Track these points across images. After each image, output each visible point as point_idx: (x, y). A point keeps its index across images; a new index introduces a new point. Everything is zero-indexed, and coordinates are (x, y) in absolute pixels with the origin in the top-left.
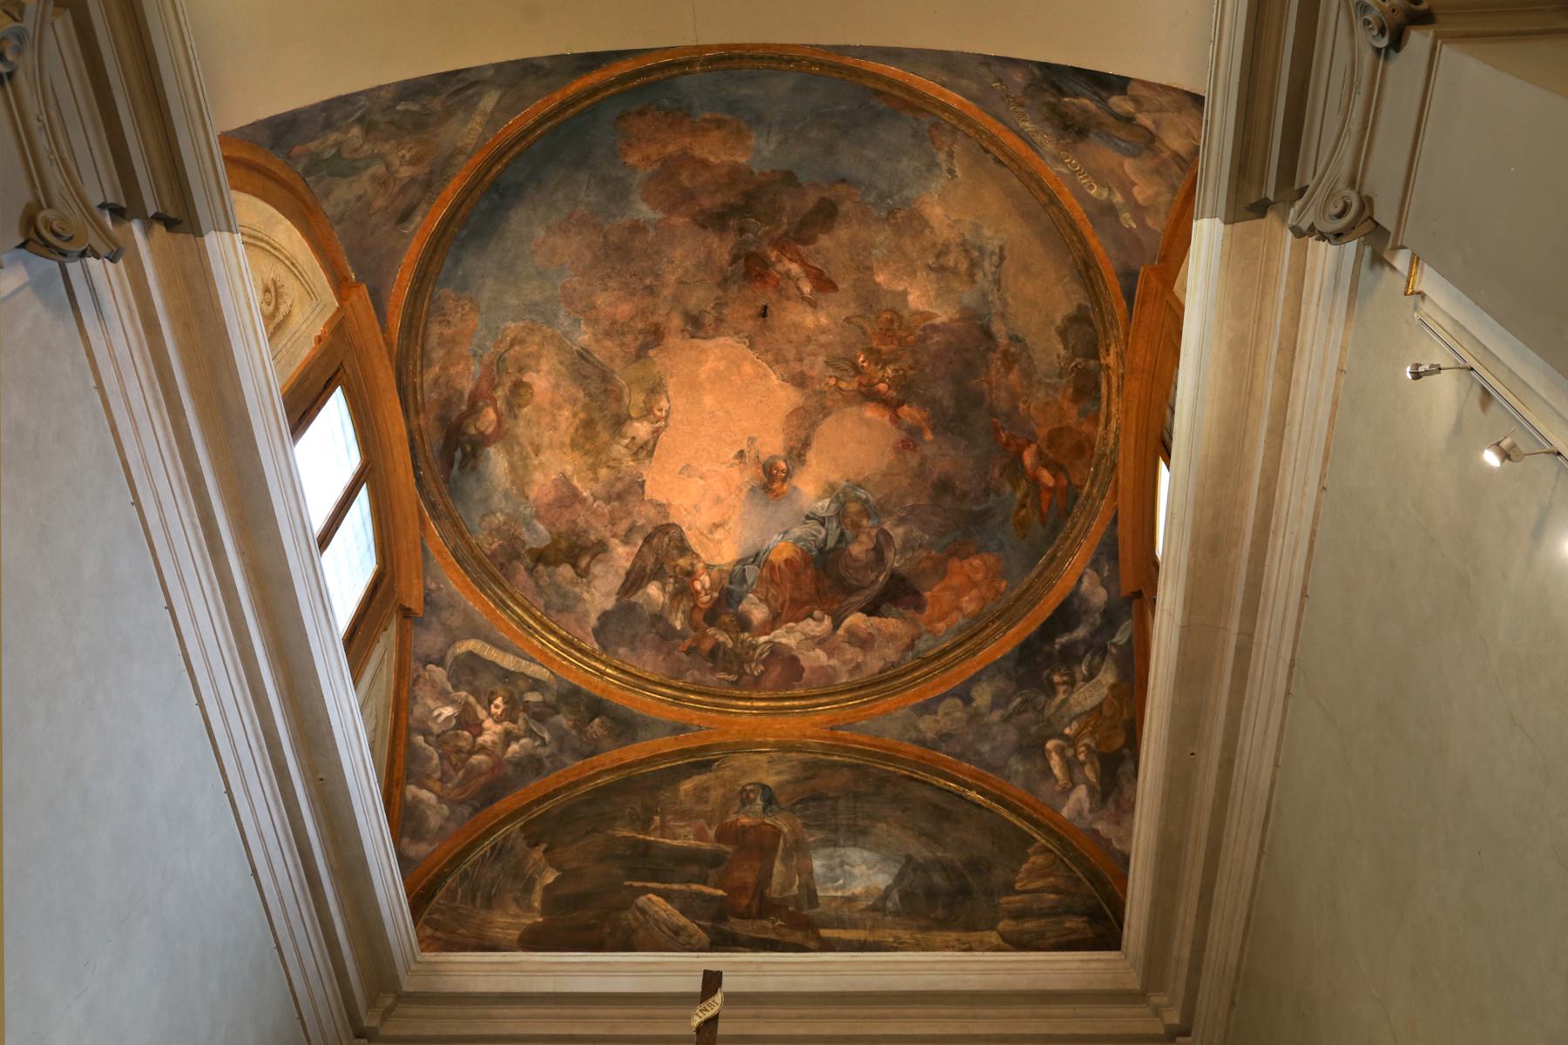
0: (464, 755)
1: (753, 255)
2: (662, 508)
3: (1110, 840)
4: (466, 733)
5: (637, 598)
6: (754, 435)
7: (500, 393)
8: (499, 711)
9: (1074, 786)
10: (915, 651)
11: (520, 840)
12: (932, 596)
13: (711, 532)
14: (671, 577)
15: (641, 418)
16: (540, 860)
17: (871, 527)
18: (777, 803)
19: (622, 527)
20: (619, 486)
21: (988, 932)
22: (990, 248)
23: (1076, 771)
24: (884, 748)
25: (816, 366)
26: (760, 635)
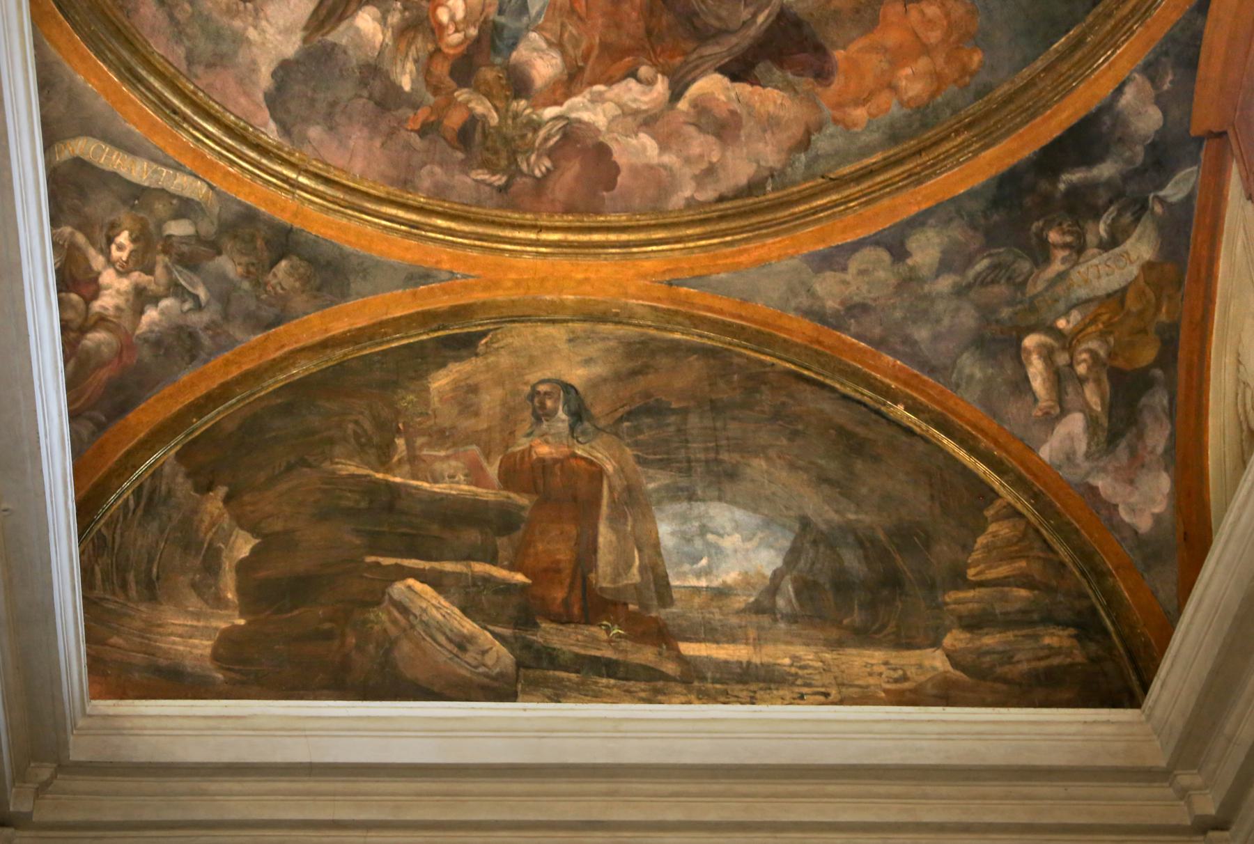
3: (1116, 506)
5: (339, 35)
8: (124, 255)
9: (1064, 412)
10: (812, 153)
11: (180, 479)
12: (847, 59)
16: (221, 515)
18: (591, 418)
21: (929, 651)
23: (1070, 390)
24: (755, 322)
26: (546, 105)
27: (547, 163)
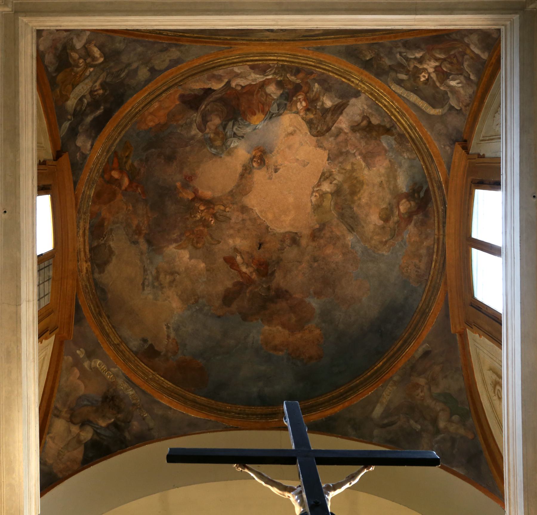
0: (449, 60)
1: (263, 276)
2: (320, 145)
4: (445, 69)
5: (337, 101)
6: (269, 181)
7: (396, 219)
8: (423, 74)
9: (84, 47)
13: (295, 131)
14: (318, 109)
15: (326, 193)
17: (208, 133)
19: (341, 138)
20: (341, 159)
22: (149, 288)
25: (236, 217)
26: (271, 79)
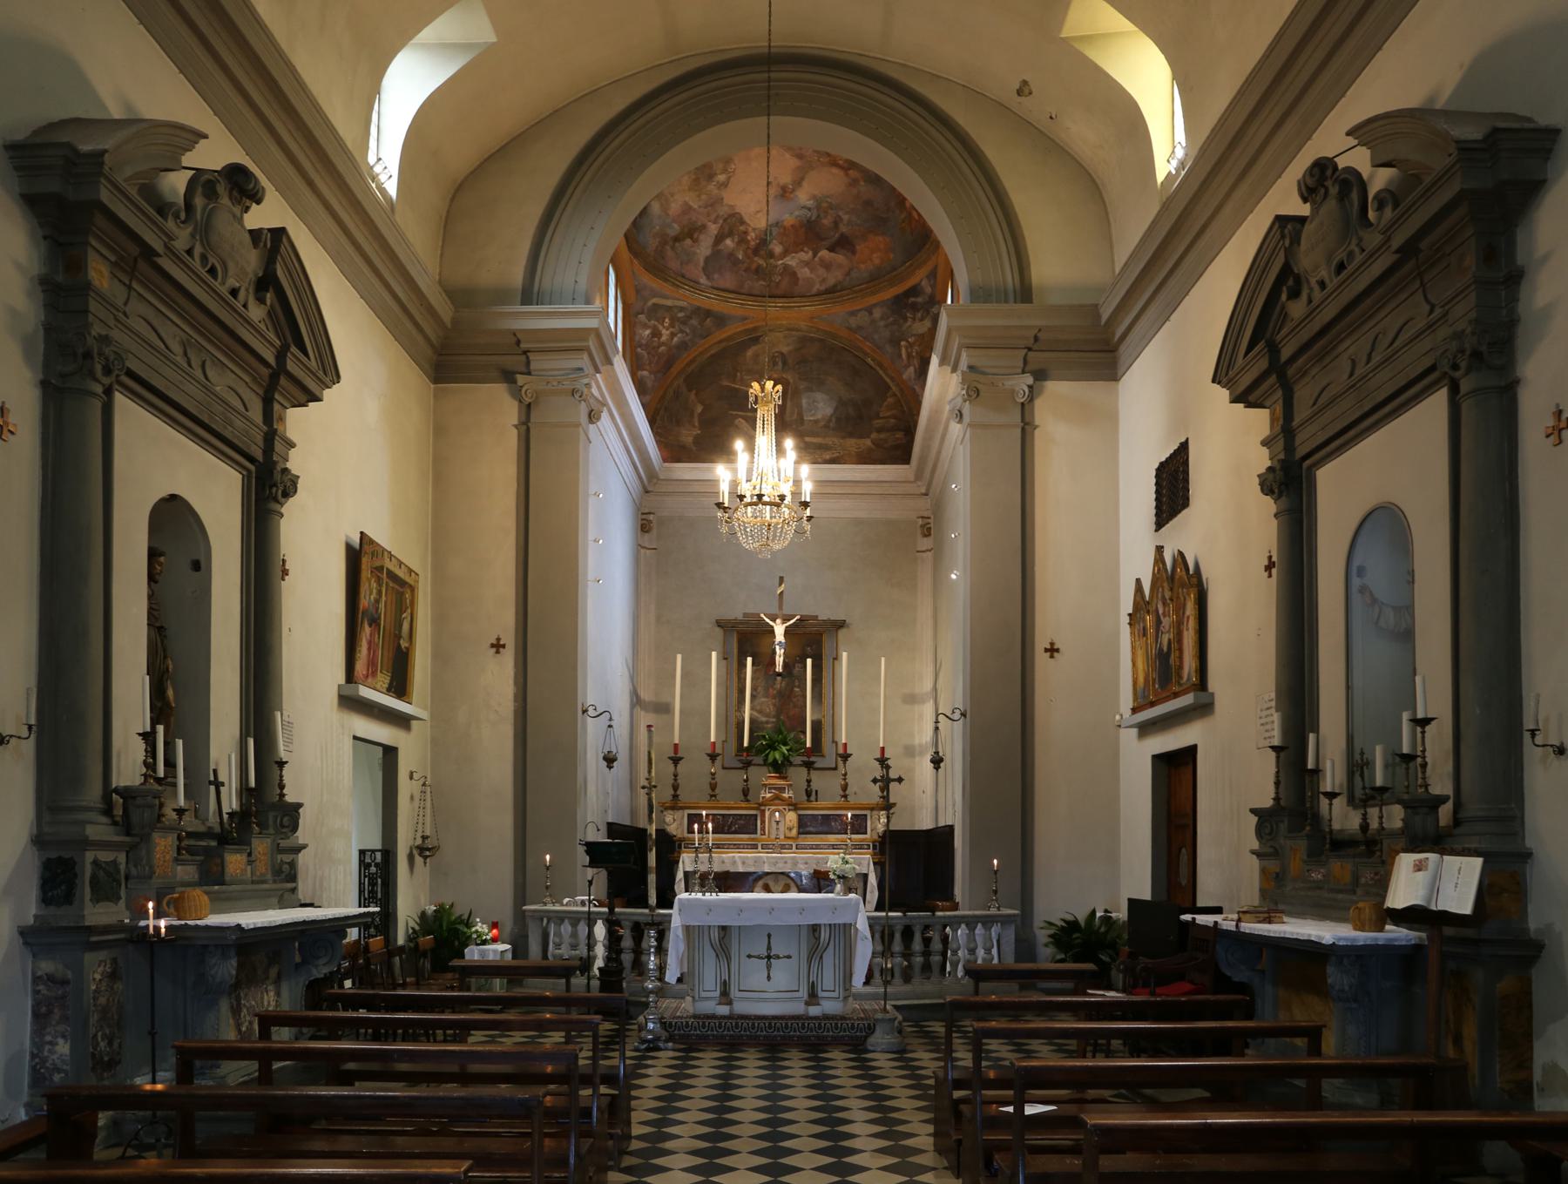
2: (732, 207)
5: (721, 247)
9: (909, 366)
13: (755, 214)
27: (780, 278)
